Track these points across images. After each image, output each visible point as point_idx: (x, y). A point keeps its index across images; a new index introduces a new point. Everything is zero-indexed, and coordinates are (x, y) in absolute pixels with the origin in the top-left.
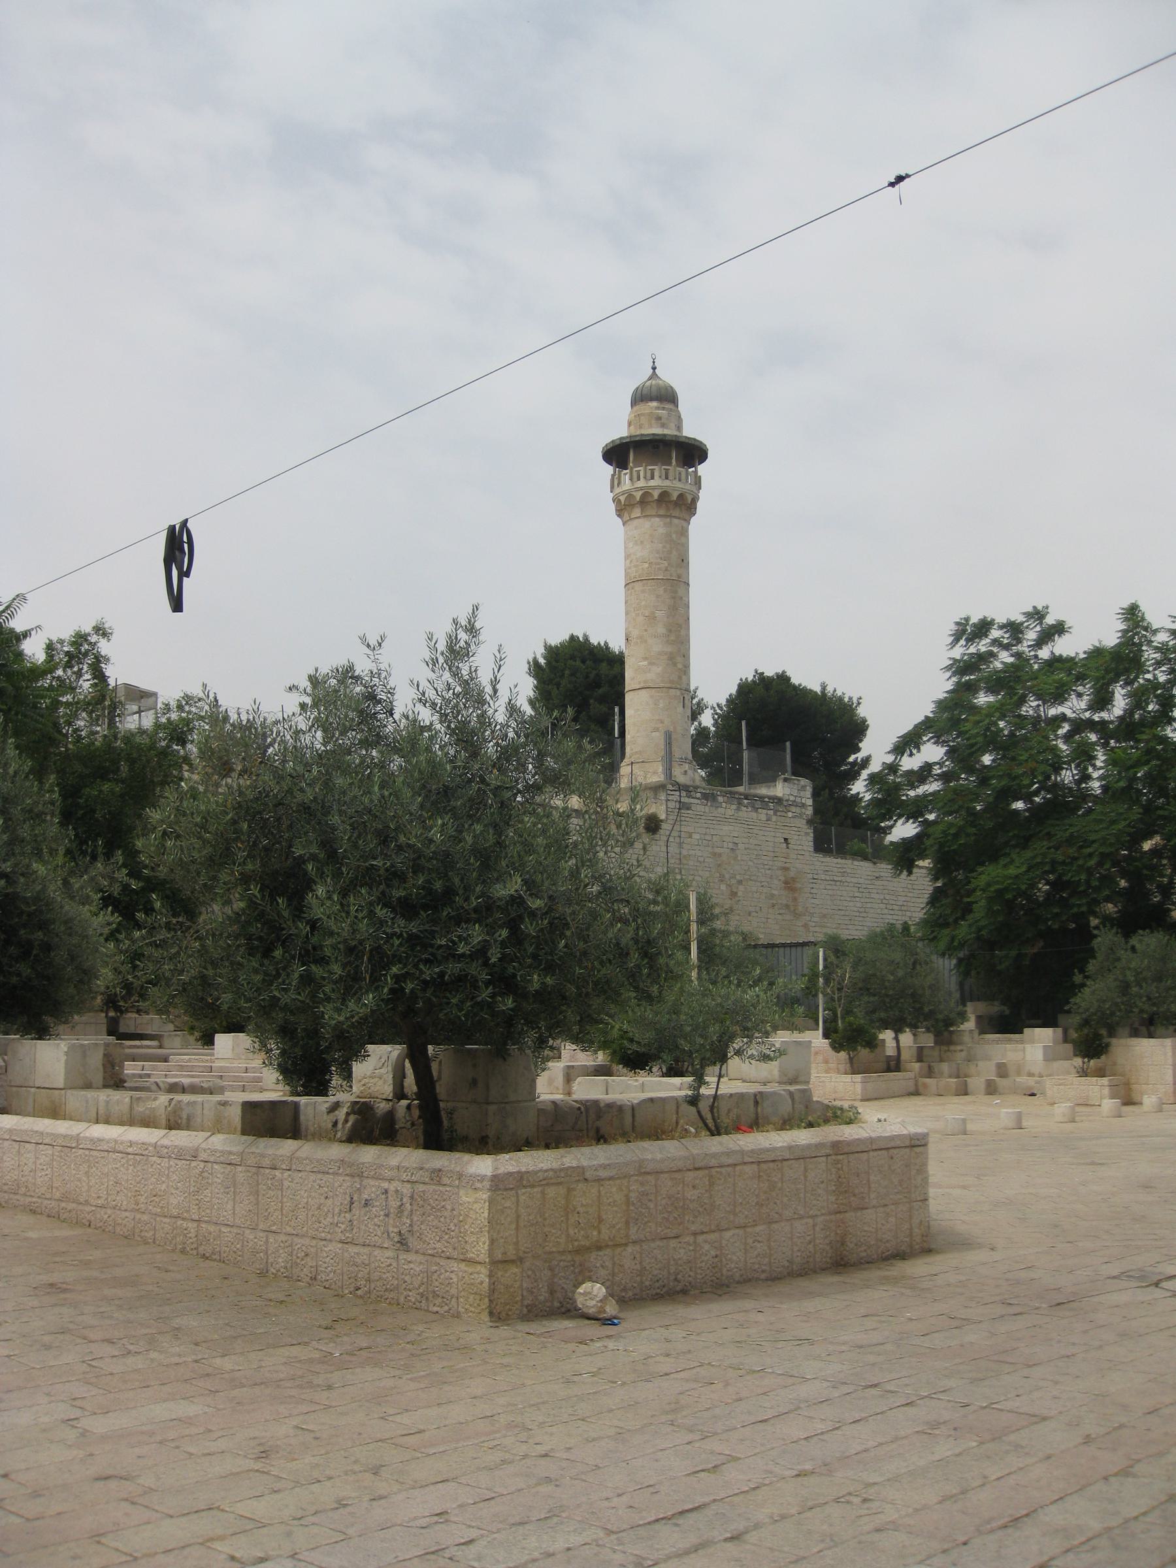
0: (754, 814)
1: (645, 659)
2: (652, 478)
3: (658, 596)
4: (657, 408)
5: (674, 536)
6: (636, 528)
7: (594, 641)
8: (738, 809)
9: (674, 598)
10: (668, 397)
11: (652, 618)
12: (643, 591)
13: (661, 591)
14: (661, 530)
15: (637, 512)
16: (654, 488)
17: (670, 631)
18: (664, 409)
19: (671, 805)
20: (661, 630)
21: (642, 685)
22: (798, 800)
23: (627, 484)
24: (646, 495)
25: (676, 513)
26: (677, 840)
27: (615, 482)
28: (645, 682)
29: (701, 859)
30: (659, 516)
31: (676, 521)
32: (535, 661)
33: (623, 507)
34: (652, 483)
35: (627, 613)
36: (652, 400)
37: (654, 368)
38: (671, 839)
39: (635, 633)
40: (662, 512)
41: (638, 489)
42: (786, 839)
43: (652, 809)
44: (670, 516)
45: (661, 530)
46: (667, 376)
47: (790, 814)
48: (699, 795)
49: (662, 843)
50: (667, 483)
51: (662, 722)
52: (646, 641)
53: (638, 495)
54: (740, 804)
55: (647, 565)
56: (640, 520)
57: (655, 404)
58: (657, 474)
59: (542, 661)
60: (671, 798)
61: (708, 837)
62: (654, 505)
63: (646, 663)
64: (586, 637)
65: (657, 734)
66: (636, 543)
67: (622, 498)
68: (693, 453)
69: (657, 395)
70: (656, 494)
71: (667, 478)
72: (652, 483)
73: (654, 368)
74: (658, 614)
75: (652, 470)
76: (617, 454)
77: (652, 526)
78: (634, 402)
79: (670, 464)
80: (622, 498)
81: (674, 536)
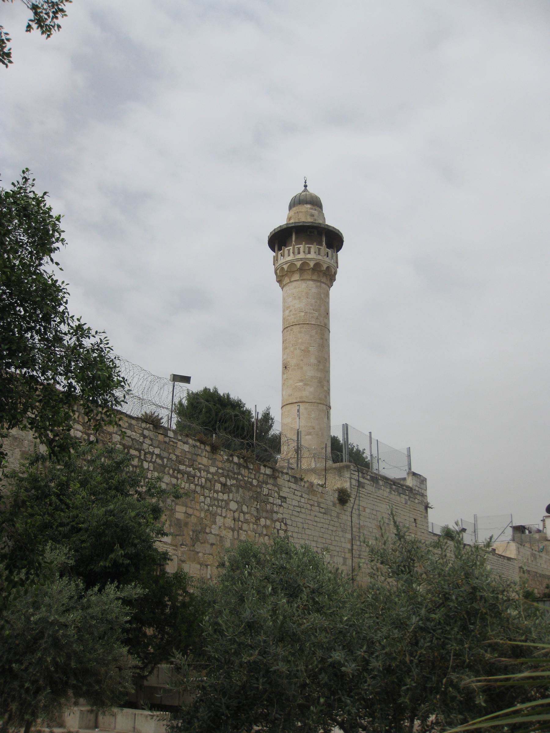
0: (398, 498)
1: (302, 381)
2: (309, 253)
3: (311, 336)
4: (312, 209)
5: (322, 296)
6: (295, 288)
7: (221, 392)
8: (390, 492)
9: (322, 339)
10: (315, 203)
11: (306, 351)
12: (300, 332)
13: (313, 333)
14: (314, 290)
15: (296, 276)
16: (311, 259)
17: (319, 362)
18: (315, 210)
19: (354, 482)
20: (313, 360)
21: (298, 400)
22: (420, 490)
23: (281, 260)
24: (305, 263)
25: (324, 280)
26: (357, 512)
27: (276, 259)
28: (301, 397)
29: (371, 530)
30: (313, 280)
31: (323, 285)
32: (180, 403)
33: (282, 276)
34: (309, 256)
35: (285, 349)
36: (307, 203)
37: (306, 186)
38: (354, 512)
39: (293, 362)
40: (315, 277)
41: (298, 260)
42: (415, 520)
43: (338, 485)
44: (321, 282)
45: (314, 290)
46: (313, 190)
47: (417, 501)
48: (369, 477)
49: (348, 513)
50: (320, 257)
51: (314, 429)
52: (302, 368)
53: (298, 264)
54: (391, 488)
55: (303, 314)
56: (299, 283)
57: (309, 206)
58: (312, 251)
59: (185, 402)
60: (353, 477)
61: (375, 513)
62: (310, 272)
63: (301, 384)
64: (216, 391)
65: (310, 437)
66: (295, 298)
67: (285, 267)
68: (333, 240)
69: (308, 201)
70: (312, 264)
71: (319, 254)
72: (309, 256)
73: (306, 186)
74: (311, 349)
75: (309, 248)
76: (279, 240)
77: (302, 287)
78: (290, 208)
79: (321, 245)
80: (285, 267)
81: (322, 296)
